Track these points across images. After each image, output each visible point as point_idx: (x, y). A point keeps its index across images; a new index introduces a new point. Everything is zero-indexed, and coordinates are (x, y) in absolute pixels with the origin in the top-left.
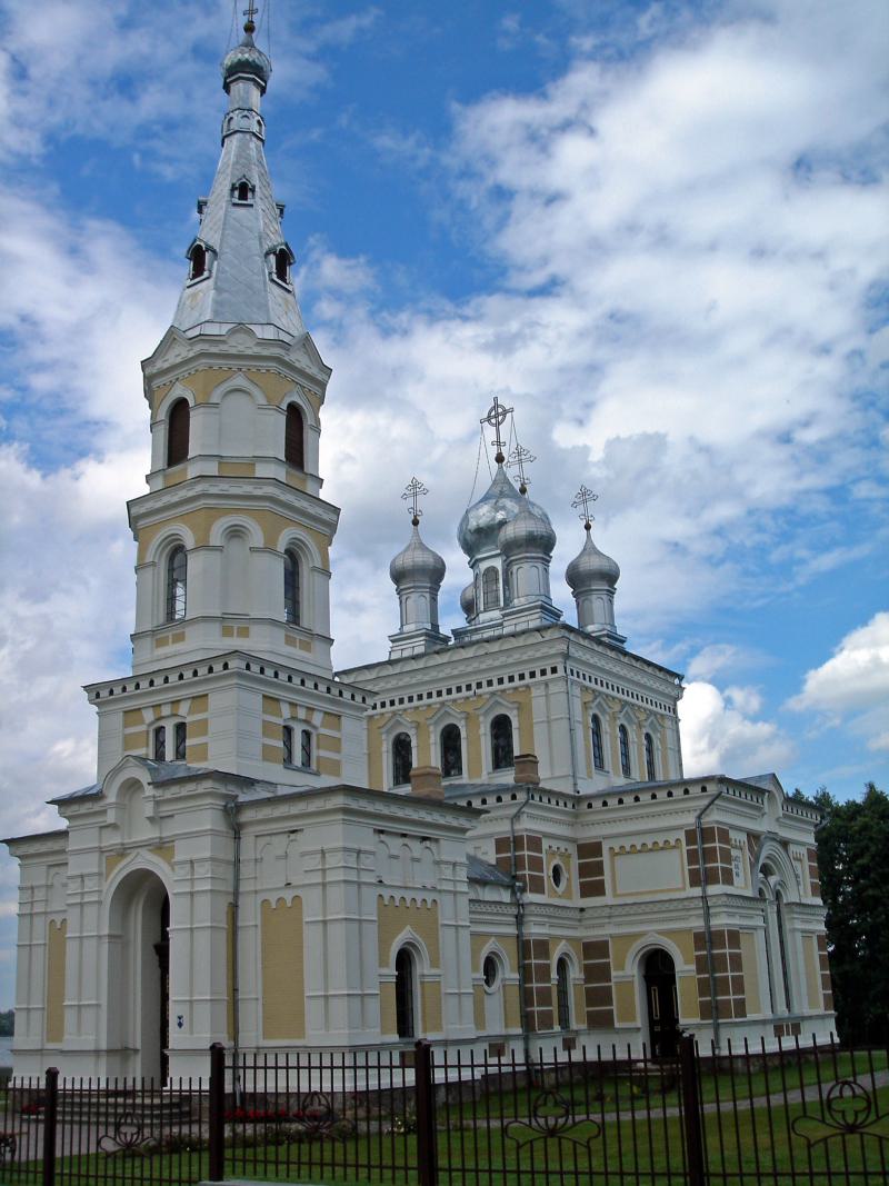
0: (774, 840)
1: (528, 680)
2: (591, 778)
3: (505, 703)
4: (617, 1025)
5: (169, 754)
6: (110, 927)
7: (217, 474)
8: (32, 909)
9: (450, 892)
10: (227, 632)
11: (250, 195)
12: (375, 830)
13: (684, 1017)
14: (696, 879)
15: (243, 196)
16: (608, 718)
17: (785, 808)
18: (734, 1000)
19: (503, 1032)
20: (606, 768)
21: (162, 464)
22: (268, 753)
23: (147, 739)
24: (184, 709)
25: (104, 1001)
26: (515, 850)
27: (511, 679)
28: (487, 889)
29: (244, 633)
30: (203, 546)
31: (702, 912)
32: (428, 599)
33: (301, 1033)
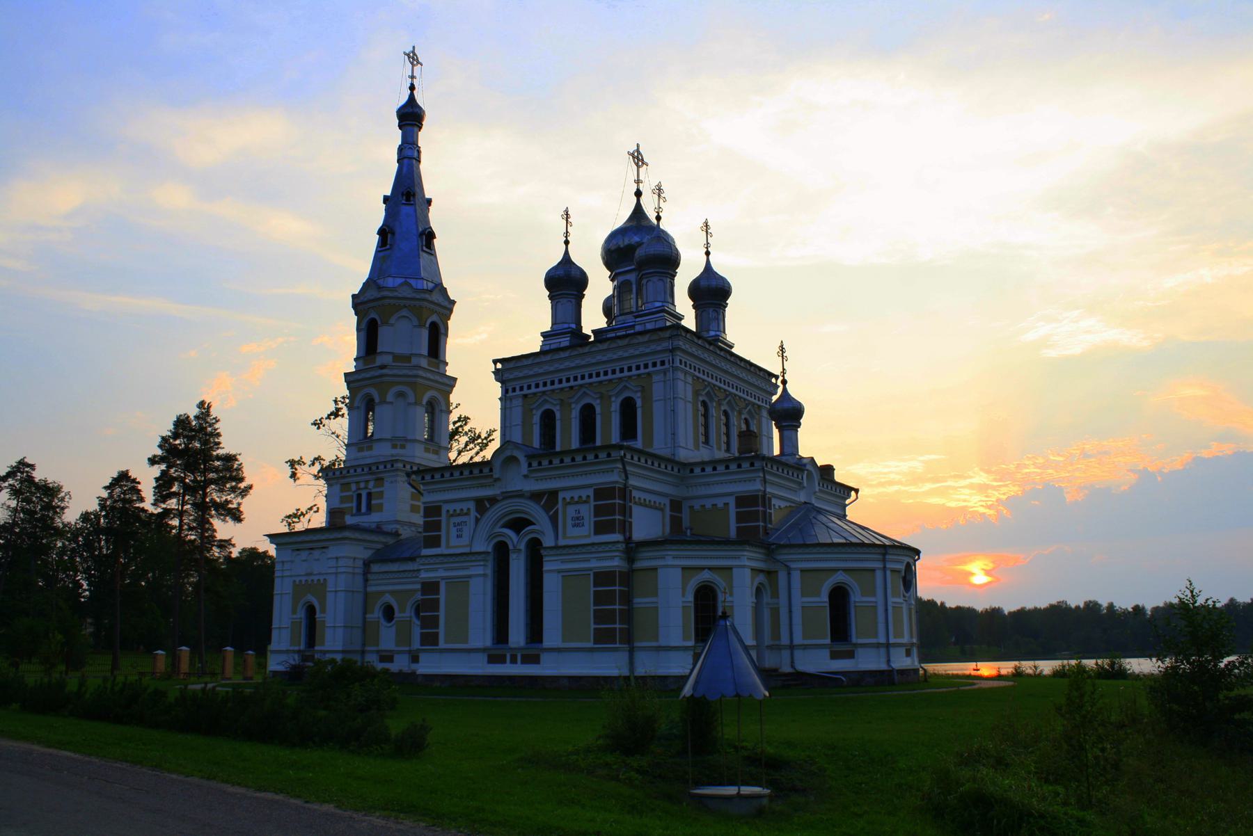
1: (651, 369)
2: (698, 450)
3: (632, 387)
10: (394, 447)
11: (412, 198)
12: (293, 550)
15: (408, 199)
16: (714, 404)
17: (821, 485)
20: (711, 443)
21: (363, 354)
24: (371, 484)
27: (638, 368)
32: (574, 303)
33: (437, 645)
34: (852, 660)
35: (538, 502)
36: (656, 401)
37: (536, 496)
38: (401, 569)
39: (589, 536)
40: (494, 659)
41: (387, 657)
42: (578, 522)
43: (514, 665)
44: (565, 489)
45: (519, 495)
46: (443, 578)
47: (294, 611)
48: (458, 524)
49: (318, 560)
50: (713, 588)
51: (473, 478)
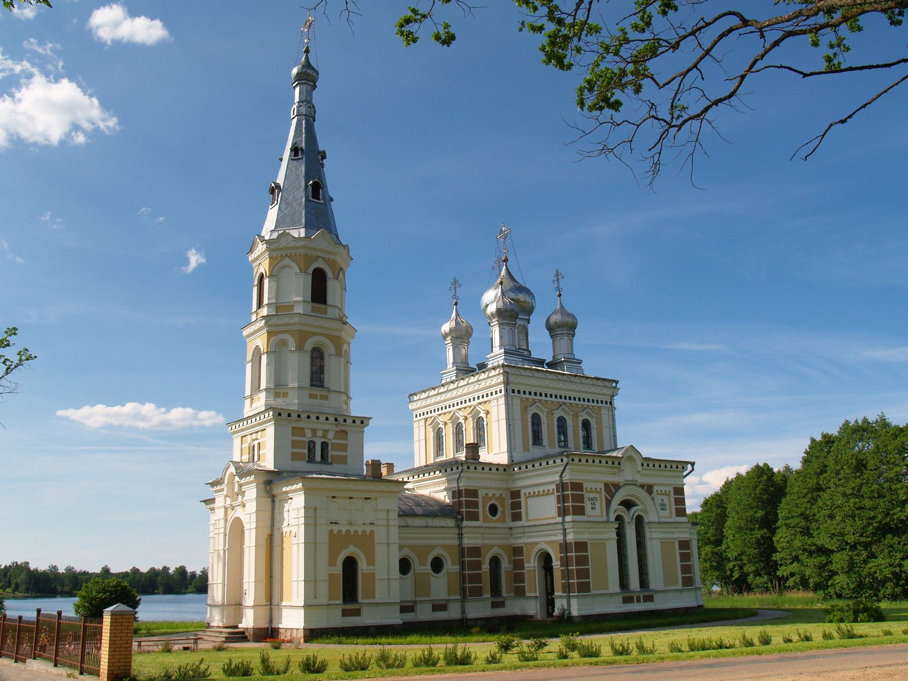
0: (636, 485)
4: (528, 594)
5: (256, 459)
13: (529, 592)
14: (563, 512)
19: (447, 598)
20: (544, 444)
22: (295, 457)
26: (459, 498)
31: (562, 531)
33: (607, 588)
35: (643, 488)
37: (642, 486)
39: (555, 518)
40: (627, 600)
42: (663, 507)
45: (633, 483)
47: (332, 563)
48: (592, 499)
51: (601, 466)
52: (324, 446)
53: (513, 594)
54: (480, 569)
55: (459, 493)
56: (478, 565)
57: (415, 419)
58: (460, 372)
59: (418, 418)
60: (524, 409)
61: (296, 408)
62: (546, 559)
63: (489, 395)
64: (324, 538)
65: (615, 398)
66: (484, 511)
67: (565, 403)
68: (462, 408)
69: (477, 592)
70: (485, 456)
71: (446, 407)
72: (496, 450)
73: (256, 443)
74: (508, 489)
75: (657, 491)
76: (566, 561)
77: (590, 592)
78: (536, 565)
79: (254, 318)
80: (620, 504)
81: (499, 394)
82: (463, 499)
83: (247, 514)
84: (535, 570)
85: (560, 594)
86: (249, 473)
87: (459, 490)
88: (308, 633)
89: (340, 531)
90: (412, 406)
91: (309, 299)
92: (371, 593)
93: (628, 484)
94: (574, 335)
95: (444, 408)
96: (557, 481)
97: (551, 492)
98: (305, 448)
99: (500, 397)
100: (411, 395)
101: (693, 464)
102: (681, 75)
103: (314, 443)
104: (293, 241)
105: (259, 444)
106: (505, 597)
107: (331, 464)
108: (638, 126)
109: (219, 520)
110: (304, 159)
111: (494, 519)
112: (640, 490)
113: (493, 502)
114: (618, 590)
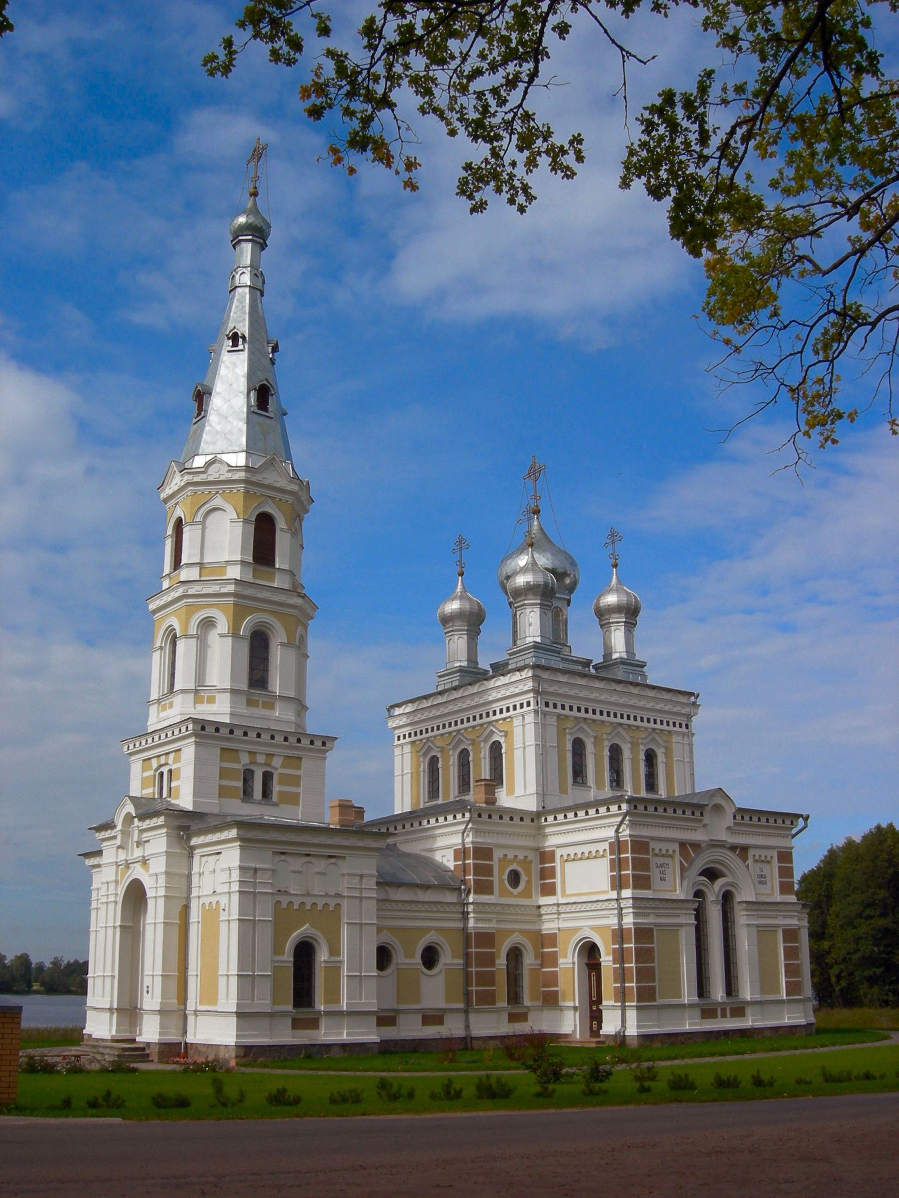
5: (165, 795)
6: (122, 919)
7: (197, 578)
8: (230, 889)
9: (357, 897)
12: (274, 852)
18: (476, 990)
22: (224, 792)
23: (155, 781)
25: (116, 973)
28: (429, 892)
29: (211, 700)
30: (186, 636)
31: (616, 912)
34: (394, 1028)
36: (517, 748)
37: (733, 848)
38: (432, 900)
39: (606, 892)
40: (708, 1013)
41: (432, 1018)
43: (725, 1019)
44: (653, 839)
45: (721, 845)
46: (656, 925)
47: (278, 949)
48: (661, 866)
49: (299, 872)
50: (389, 951)
52: (267, 777)
53: (539, 1003)
54: (493, 964)
55: (464, 852)
56: (490, 960)
57: (397, 743)
58: (465, 674)
59: (402, 741)
60: (561, 733)
61: (226, 719)
62: (590, 951)
63: (511, 708)
64: (264, 914)
65: (692, 719)
66: (501, 881)
67: (621, 724)
68: (469, 727)
69: (488, 998)
70: (505, 799)
71: (456, 722)
72: (519, 790)
73: (165, 770)
74: (537, 849)
75: (754, 856)
76: (620, 956)
77: (655, 1000)
78: (576, 960)
79: (166, 584)
80: (701, 874)
81: (525, 709)
82: (470, 861)
83: (151, 875)
84: (574, 968)
85: (612, 1003)
86: (156, 814)
87: (464, 848)
88: (242, 1053)
89: (314, 904)
90: (392, 724)
91: (250, 559)
92: (333, 995)
93: (713, 846)
94: (635, 625)
95: (430, 730)
96: (611, 838)
97: (601, 853)
98: (238, 780)
99: (528, 712)
100: (393, 707)
101: (806, 818)
102: (855, 254)
103: (252, 772)
104: (229, 471)
105: (170, 771)
106: (528, 1007)
107: (276, 805)
108: (812, 327)
109: (108, 883)
110: (246, 350)
111: (515, 891)
112: (729, 853)
113: (514, 866)
114: (695, 999)
